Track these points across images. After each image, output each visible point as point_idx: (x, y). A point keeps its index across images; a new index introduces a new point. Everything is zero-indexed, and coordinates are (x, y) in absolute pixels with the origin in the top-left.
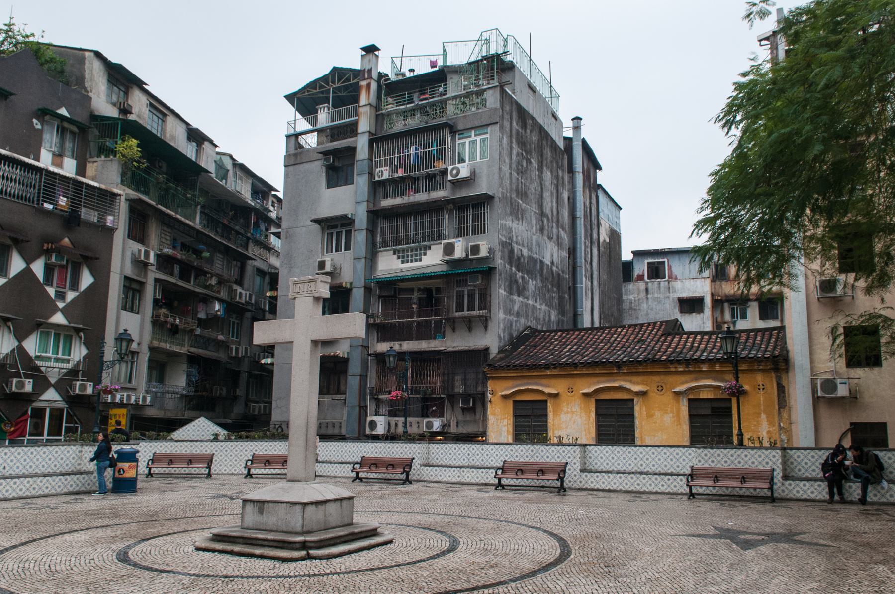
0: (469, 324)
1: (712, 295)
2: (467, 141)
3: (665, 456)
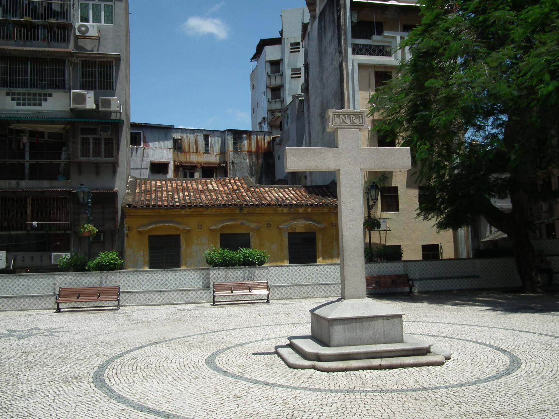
1: (174, 161)
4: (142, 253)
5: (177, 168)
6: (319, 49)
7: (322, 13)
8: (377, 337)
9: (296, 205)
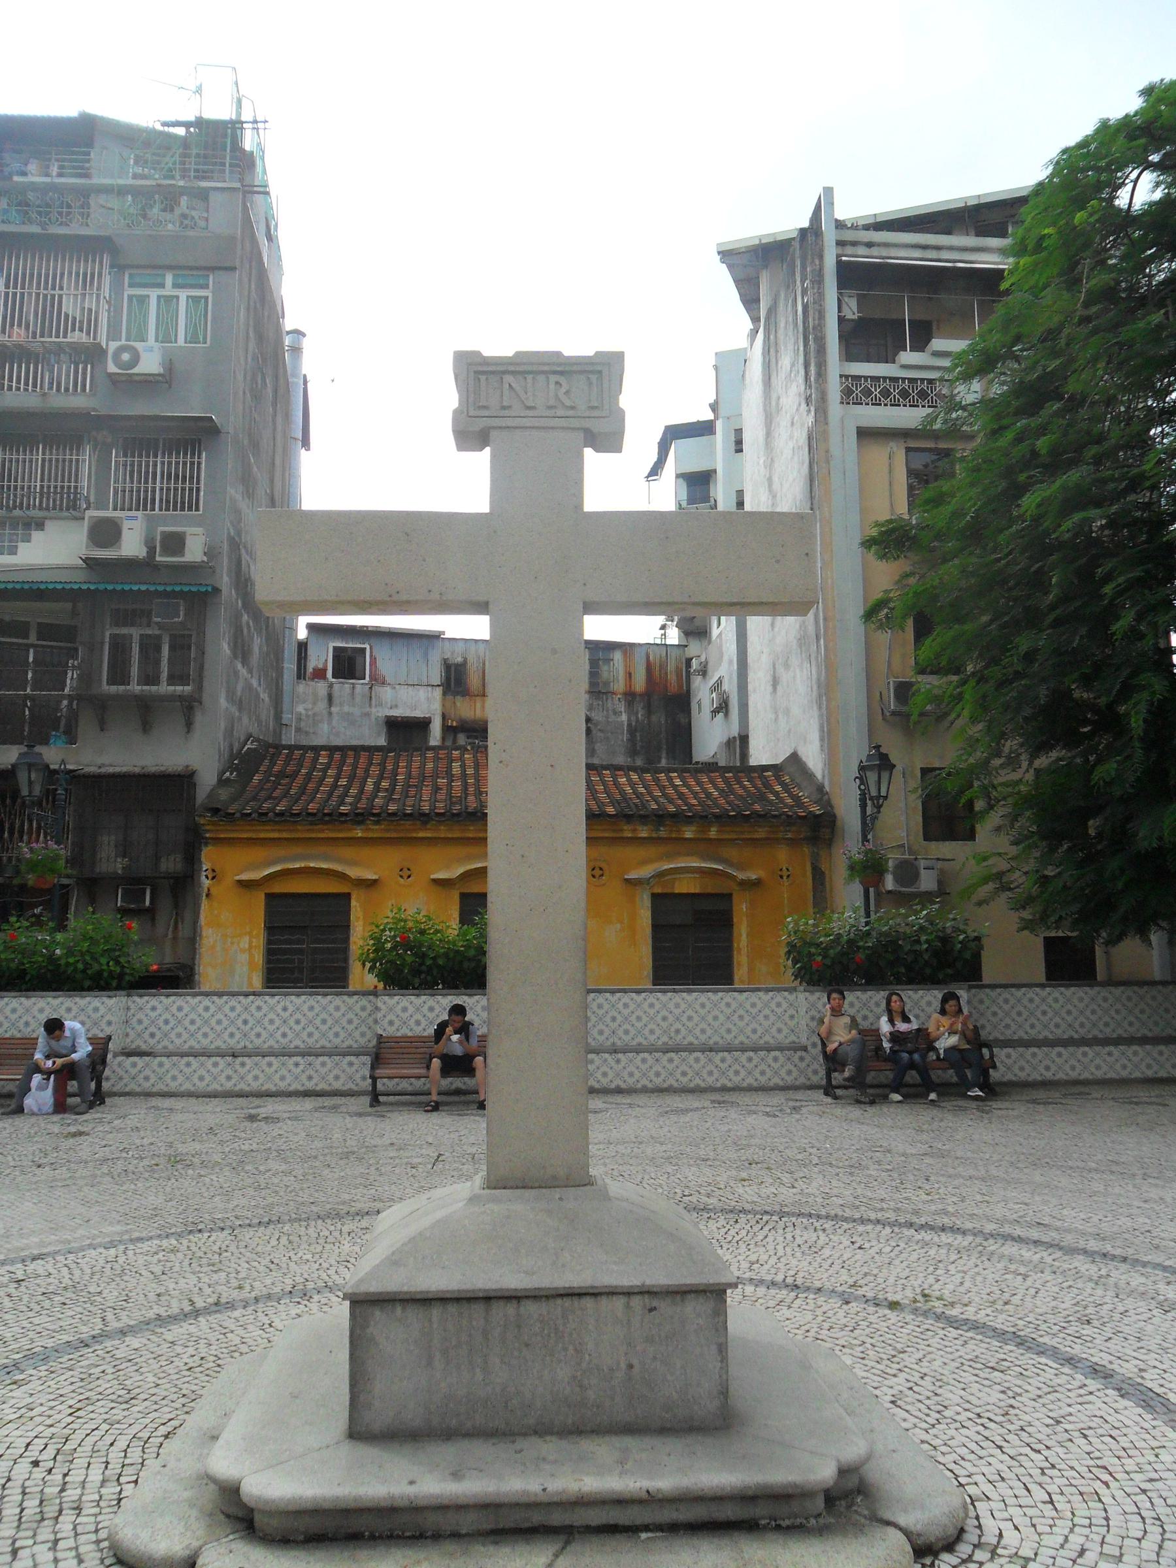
0: (146, 714)
2: (153, 294)
3: (728, 1011)
4: (245, 942)
5: (447, 730)
6: (765, 405)
7: (772, 311)
8: (591, 1394)
9: (674, 816)
